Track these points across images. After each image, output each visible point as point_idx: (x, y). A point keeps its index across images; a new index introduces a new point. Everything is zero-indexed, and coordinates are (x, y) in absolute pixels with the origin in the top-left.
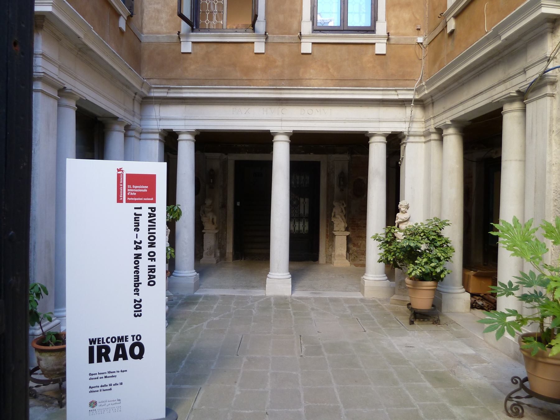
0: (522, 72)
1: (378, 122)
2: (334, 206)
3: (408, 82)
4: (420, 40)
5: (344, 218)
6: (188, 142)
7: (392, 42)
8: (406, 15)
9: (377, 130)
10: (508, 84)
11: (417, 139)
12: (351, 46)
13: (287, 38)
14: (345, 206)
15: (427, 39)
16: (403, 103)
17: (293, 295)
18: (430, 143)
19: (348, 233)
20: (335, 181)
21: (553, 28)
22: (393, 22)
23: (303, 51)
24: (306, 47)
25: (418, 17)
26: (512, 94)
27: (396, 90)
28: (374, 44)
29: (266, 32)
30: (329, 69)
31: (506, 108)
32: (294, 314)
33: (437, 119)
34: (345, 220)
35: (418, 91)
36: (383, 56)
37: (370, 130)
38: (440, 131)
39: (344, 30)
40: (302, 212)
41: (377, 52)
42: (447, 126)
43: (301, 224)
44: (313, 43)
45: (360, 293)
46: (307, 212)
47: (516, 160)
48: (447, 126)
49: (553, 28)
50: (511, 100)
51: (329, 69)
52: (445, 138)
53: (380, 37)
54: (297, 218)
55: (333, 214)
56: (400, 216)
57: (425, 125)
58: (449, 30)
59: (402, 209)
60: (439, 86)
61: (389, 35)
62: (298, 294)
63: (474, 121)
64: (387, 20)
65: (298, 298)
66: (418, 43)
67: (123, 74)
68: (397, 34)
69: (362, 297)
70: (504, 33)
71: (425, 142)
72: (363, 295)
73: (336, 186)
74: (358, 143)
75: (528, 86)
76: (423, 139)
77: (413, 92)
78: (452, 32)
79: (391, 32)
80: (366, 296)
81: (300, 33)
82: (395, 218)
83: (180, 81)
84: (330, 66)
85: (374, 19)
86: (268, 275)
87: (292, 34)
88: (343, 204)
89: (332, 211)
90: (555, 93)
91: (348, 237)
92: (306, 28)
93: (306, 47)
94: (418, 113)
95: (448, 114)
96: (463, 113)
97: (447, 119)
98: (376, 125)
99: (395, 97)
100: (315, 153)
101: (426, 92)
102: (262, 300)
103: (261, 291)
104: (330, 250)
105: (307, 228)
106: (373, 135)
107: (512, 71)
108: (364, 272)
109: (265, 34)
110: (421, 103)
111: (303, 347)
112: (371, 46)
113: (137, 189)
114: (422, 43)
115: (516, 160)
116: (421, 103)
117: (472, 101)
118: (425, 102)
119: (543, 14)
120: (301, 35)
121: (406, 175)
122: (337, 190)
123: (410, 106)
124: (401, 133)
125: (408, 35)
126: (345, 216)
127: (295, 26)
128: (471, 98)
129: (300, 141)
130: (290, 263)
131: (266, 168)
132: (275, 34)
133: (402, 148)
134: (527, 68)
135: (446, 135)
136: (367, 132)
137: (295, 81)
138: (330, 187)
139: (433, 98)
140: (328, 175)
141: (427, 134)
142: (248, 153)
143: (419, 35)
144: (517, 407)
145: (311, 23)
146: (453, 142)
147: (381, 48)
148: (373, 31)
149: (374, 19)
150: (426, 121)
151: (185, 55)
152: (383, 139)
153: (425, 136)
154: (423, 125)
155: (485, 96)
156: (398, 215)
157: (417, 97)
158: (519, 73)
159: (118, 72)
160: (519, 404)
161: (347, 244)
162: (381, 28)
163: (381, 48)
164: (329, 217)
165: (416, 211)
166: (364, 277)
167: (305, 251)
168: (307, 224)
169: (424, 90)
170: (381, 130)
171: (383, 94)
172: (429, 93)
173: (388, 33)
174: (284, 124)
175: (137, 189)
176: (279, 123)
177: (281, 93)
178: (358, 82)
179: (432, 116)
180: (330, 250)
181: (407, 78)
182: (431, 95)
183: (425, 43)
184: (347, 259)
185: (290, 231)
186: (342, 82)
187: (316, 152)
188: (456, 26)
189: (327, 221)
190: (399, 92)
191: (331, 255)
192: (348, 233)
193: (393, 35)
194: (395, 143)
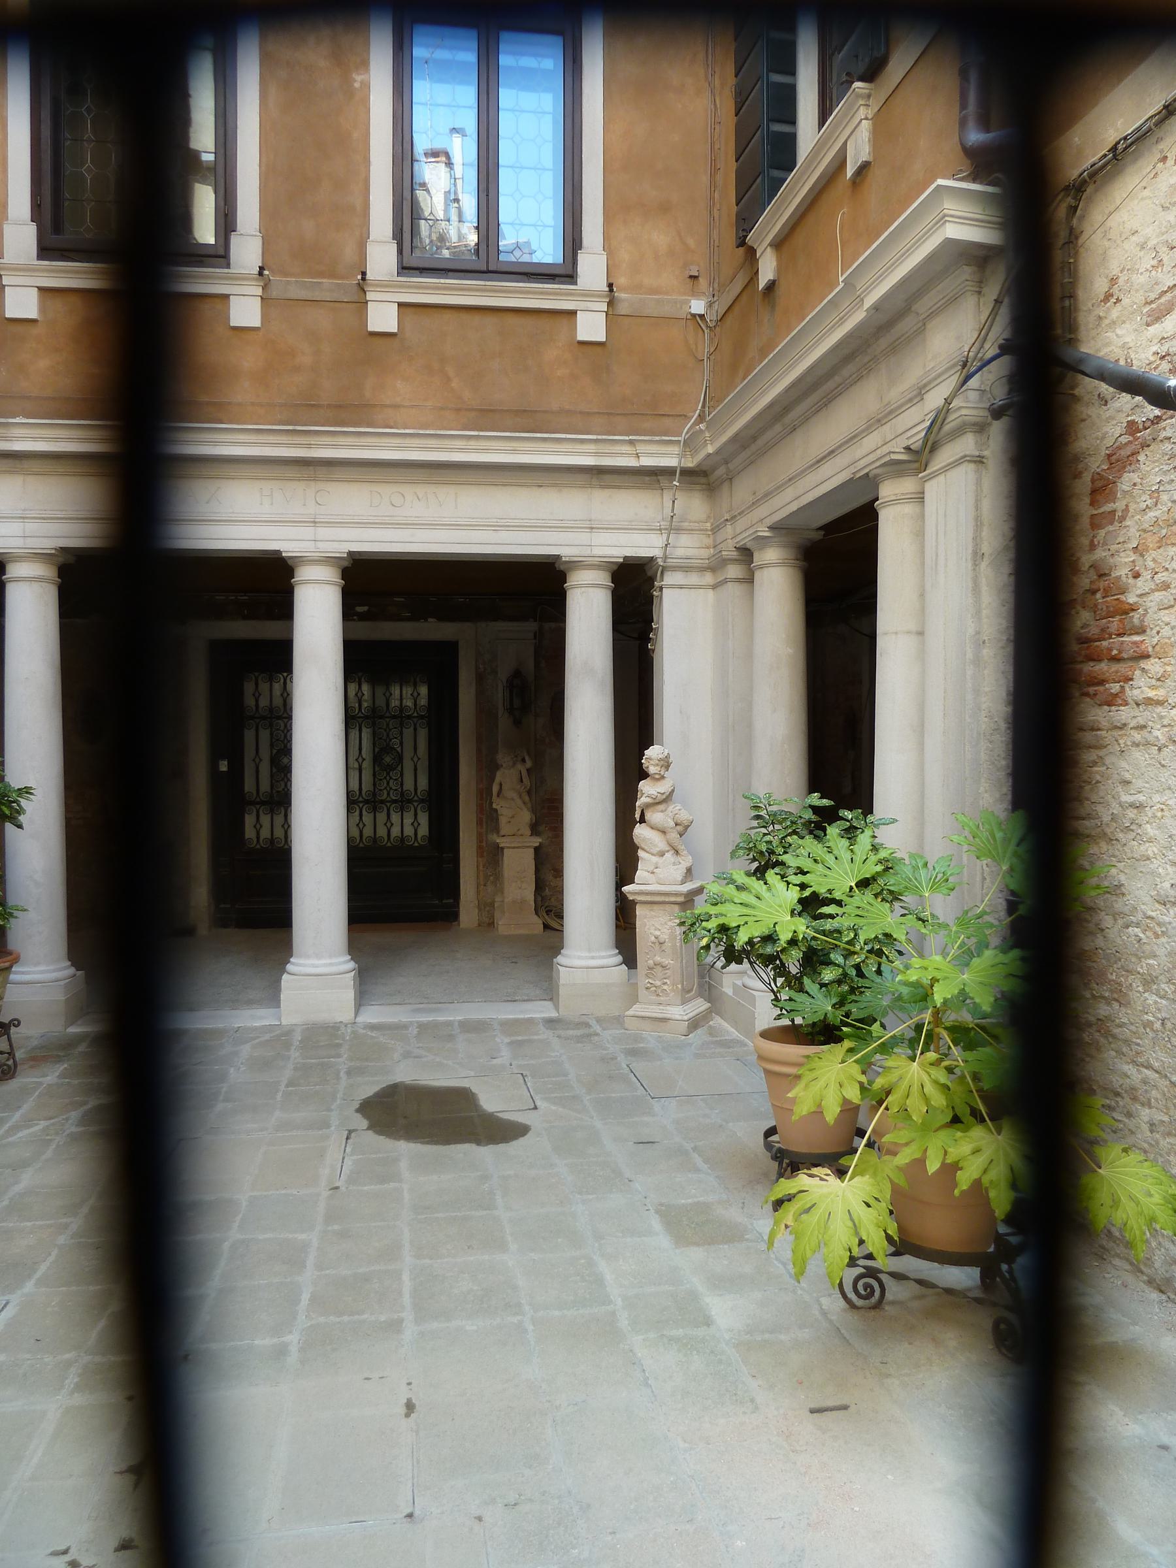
0: (916, 396)
1: (586, 532)
2: (497, 767)
3: (667, 422)
4: (698, 306)
5: (527, 798)
6: (36, 586)
7: (623, 309)
8: (659, 237)
10: (887, 430)
11: (694, 578)
12: (512, 320)
13: (326, 288)
14: (529, 764)
15: (716, 306)
16: (653, 477)
17: (360, 1019)
18: (725, 586)
19: (536, 841)
20: (499, 696)
21: (981, 282)
22: (625, 255)
23: (373, 326)
24: (382, 317)
25: (691, 242)
26: (894, 457)
27: (631, 442)
28: (573, 313)
29: (261, 269)
30: (449, 379)
31: (887, 491)
32: (349, 1073)
33: (741, 524)
34: (529, 805)
35: (689, 445)
36: (599, 349)
38: (746, 554)
39: (488, 272)
40: (409, 785)
41: (582, 336)
42: (762, 541)
43: (408, 820)
44: (400, 305)
45: (548, 1004)
46: (423, 783)
47: (909, 632)
48: (762, 541)
49: (981, 282)
50: (896, 468)
51: (449, 379)
52: (757, 575)
53: (588, 294)
54: (366, 802)
55: (495, 789)
56: (647, 790)
57: (714, 541)
58: (762, 284)
59: (652, 770)
60: (737, 435)
61: (611, 290)
62: (373, 1015)
64: (608, 246)
65: (373, 1027)
66: (694, 316)
68: (636, 288)
69: (554, 1014)
70: (868, 290)
71: (714, 587)
72: (557, 1008)
73: (501, 712)
74: (534, 588)
75: (923, 434)
76: (709, 579)
77: (676, 449)
78: (771, 286)
79: (621, 281)
80: (564, 1012)
81: (364, 274)
84: (451, 371)
85: (573, 242)
86: (289, 967)
87: (342, 278)
88: (524, 761)
89: (492, 779)
90: (986, 453)
91: (536, 849)
92: (382, 258)
93: (382, 317)
94: (693, 505)
95: (762, 511)
96: (794, 507)
97: (757, 522)
98: (583, 537)
99: (632, 462)
100: (441, 619)
101: (710, 449)
102: (267, 1037)
103: (262, 1012)
104: (490, 888)
105: (424, 830)
106: (575, 565)
107: (897, 393)
108: (556, 947)
109: (261, 274)
110: (703, 480)
111: (348, 1162)
112: (564, 321)
114: (702, 316)
115: (909, 632)
116: (698, 477)
117: (807, 478)
118: (713, 478)
119: (949, 242)
120: (364, 279)
121: (666, 677)
122: (504, 722)
123: (671, 488)
125: (667, 293)
126: (529, 793)
127: (349, 253)
128: (812, 466)
129: (370, 583)
130: (349, 930)
131: (278, 658)
132: (292, 275)
134: (925, 386)
135: (761, 567)
136: (558, 557)
137: (351, 412)
138: (485, 712)
139: (731, 466)
140: (480, 678)
141: (715, 565)
142: (245, 618)
143: (695, 294)
145: (394, 247)
147: (591, 326)
148: (570, 276)
149: (573, 242)
150: (715, 530)
151: (19, 328)
152: (604, 578)
153: (713, 569)
154: (709, 541)
155: (840, 461)
156: (642, 785)
157: (690, 463)
158: (911, 400)
159: (725, 444)
160: (872, 1273)
161: (537, 871)
162: (592, 268)
163: (591, 326)
164: (485, 795)
166: (560, 959)
167: (402, 897)
168: (424, 819)
169: (705, 444)
170: (597, 551)
171: (597, 454)
172: (717, 452)
173: (610, 286)
174: (323, 532)
176: (307, 532)
177: (309, 446)
178: (529, 419)
179: (727, 516)
180: (490, 888)
181: (666, 410)
182: (725, 456)
183: (711, 318)
184: (537, 913)
185: (350, 841)
186: (487, 417)
187: (446, 614)
188: (779, 270)
189: (481, 810)
190: (641, 448)
191: (492, 904)
192: (536, 841)
193: (623, 289)
194: (634, 589)
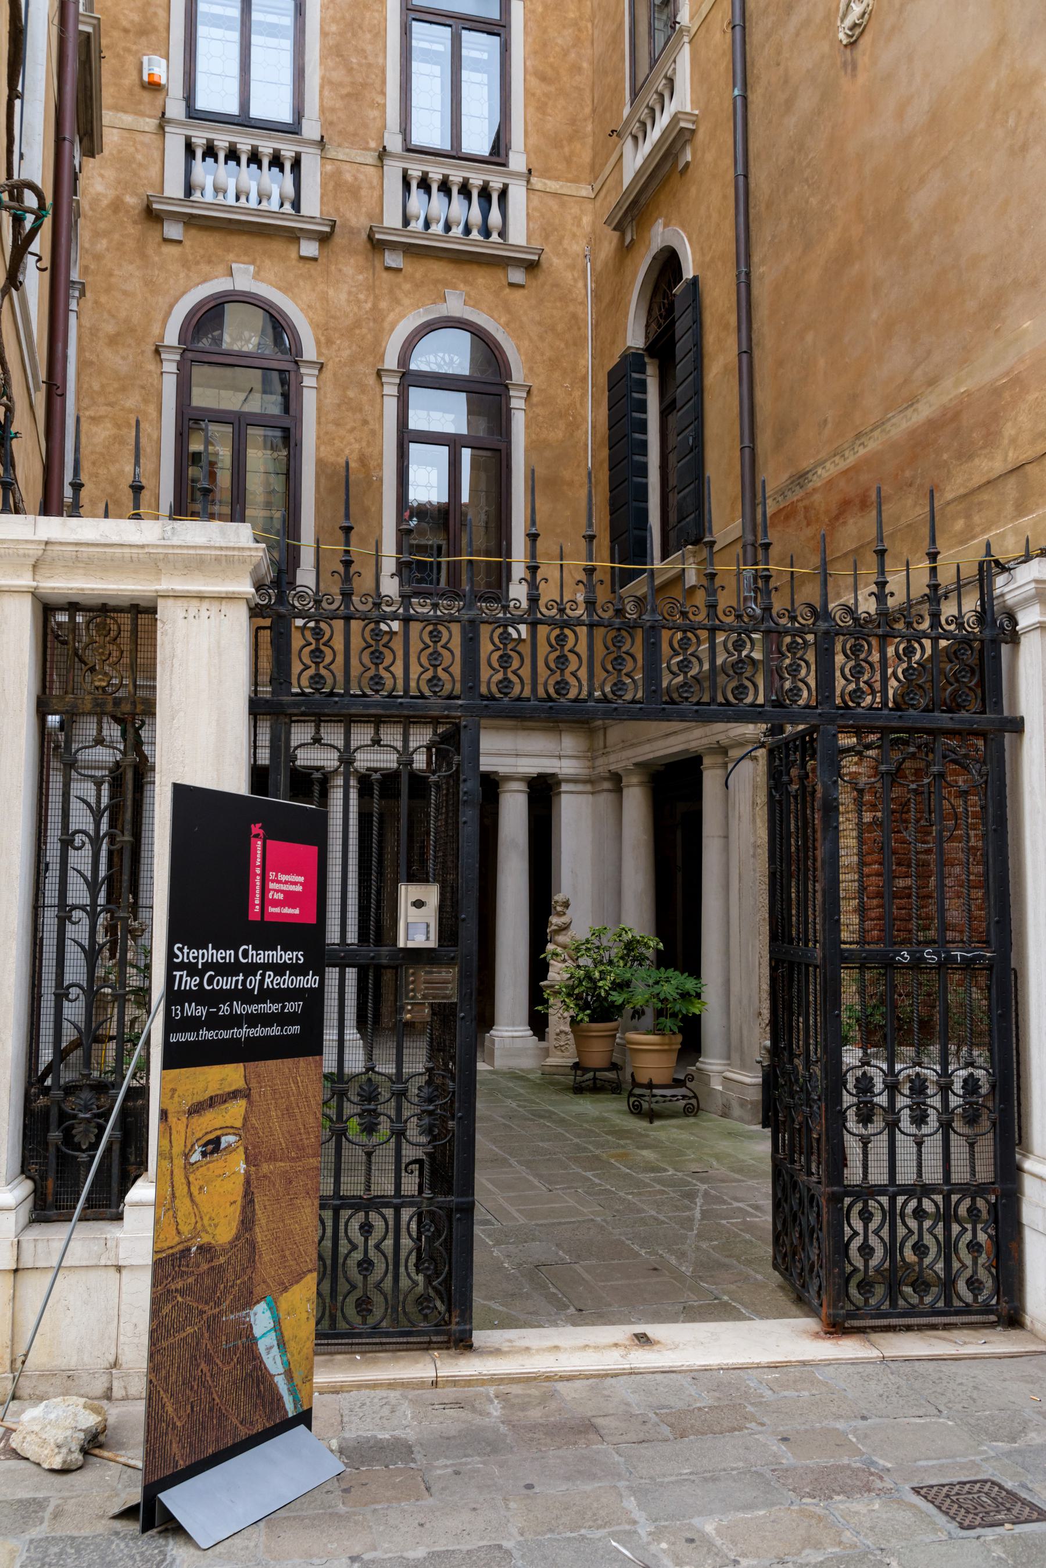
9: (513, 770)
37: (502, 770)
38: (616, 781)
63: (668, 766)
67: (122, 587)
69: (490, 1068)
71: (592, 793)
76: (588, 788)
82: (546, 923)
83: (369, 463)
95: (629, 753)
113: (286, 882)
124: (553, 775)
133: (554, 799)
144: (87, 840)
146: (636, 802)
165: (579, 914)
170: (521, 770)
175: (286, 882)
194: (542, 792)
